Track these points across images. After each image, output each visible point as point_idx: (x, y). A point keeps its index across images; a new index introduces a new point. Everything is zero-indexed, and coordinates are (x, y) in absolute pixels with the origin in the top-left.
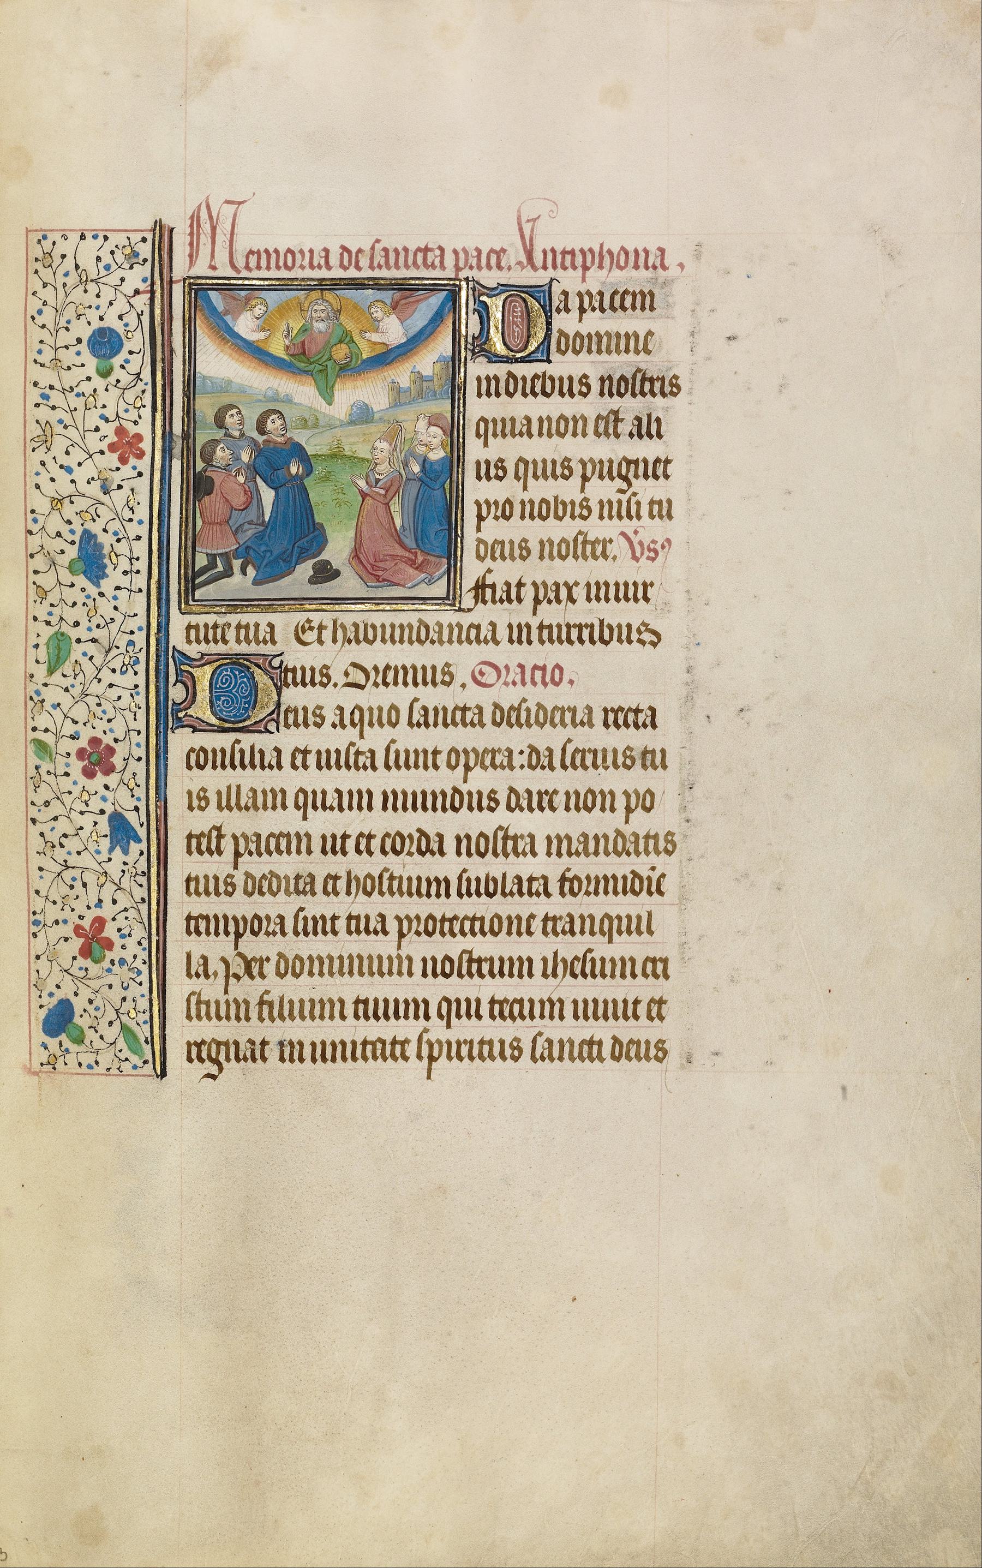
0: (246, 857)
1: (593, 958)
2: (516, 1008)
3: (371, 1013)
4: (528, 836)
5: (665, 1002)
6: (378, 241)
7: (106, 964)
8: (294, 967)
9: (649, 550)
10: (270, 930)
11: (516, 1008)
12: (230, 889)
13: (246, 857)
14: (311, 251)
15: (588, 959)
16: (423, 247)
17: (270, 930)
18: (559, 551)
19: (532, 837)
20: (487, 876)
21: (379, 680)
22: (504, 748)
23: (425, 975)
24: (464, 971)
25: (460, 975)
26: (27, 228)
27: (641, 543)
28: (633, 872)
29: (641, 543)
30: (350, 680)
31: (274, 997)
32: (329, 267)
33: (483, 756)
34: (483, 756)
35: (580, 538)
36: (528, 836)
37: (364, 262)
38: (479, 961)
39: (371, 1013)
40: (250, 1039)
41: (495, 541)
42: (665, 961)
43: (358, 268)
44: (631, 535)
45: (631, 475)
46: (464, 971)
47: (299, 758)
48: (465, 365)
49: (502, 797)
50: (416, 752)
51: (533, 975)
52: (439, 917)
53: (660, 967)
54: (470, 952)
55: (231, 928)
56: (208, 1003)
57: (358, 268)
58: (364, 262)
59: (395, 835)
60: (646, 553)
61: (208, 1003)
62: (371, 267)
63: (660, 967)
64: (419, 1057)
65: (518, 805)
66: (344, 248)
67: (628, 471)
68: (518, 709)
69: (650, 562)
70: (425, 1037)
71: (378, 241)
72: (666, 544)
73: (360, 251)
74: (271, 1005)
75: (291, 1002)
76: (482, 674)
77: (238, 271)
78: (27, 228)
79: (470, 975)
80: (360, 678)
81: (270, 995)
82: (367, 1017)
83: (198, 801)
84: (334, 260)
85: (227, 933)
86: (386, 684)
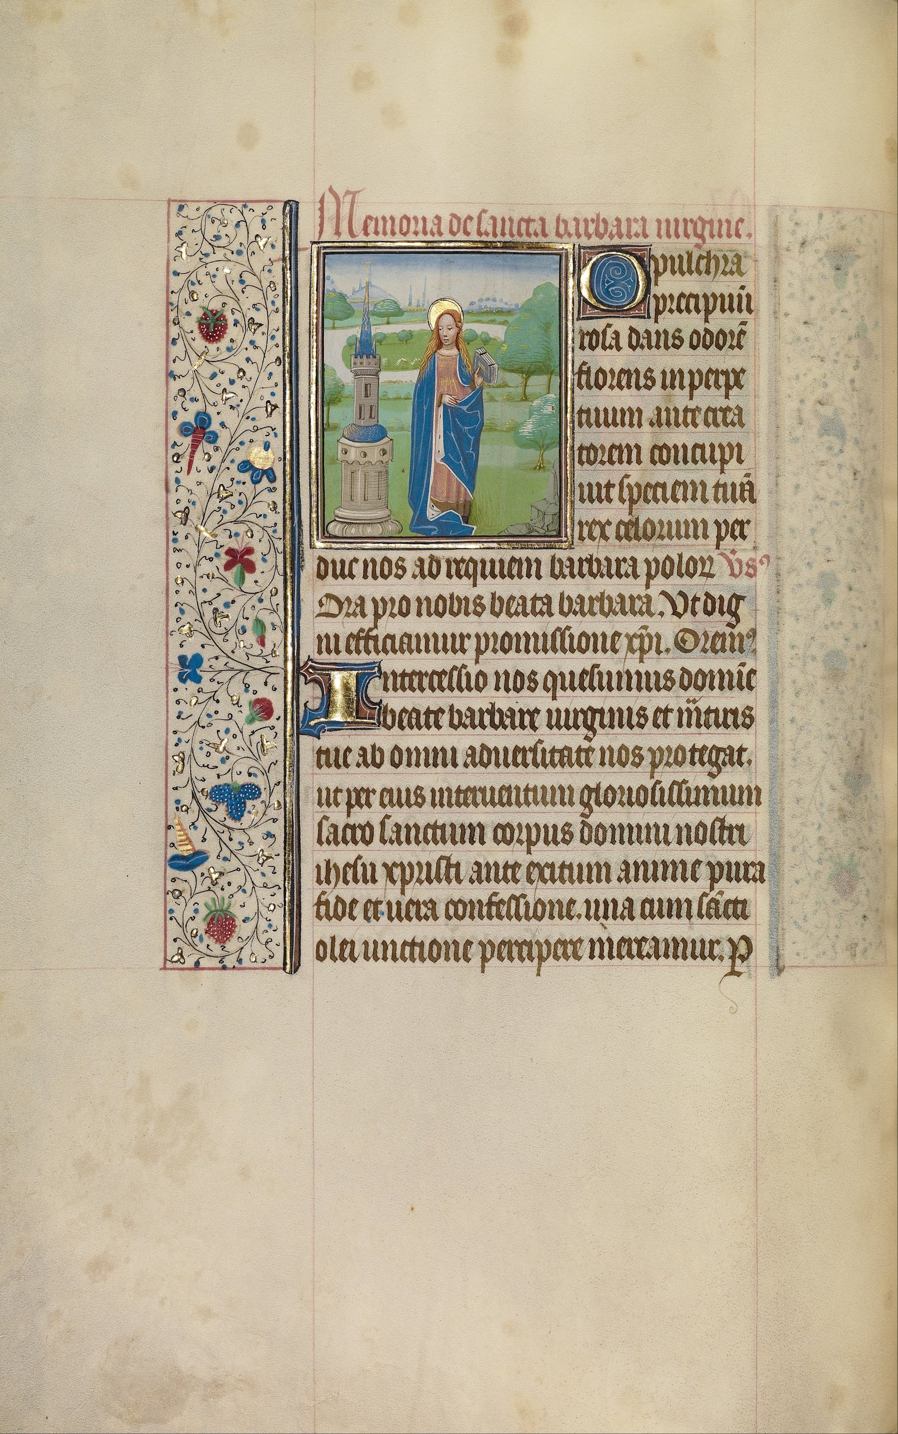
0: (666, 313)
1: (363, 863)
2: (692, 302)
4: (630, 559)
6: (484, 211)
7: (222, 551)
8: (597, 835)
10: (728, 269)
11: (692, 302)
13: (357, 808)
14: (424, 219)
16: (410, 941)
17: (728, 269)
19: (543, 220)
21: (708, 646)
24: (717, 837)
25: (713, 841)
26: (161, 969)
28: (683, 669)
30: (323, 610)
32: (495, 235)
36: (630, 559)
37: (472, 227)
38: (730, 828)
40: (628, 898)
43: (467, 233)
46: (717, 837)
48: (285, 710)
49: (487, 602)
51: (761, 803)
52: (423, 710)
54: (722, 821)
55: (717, 456)
57: (467, 233)
58: (472, 227)
59: (469, 561)
62: (479, 233)
64: (622, 500)
65: (611, 610)
66: (454, 216)
67: (589, 798)
68: (355, 866)
69: (640, 745)
70: (626, 481)
71: (484, 211)
73: (470, 218)
76: (684, 641)
78: (161, 969)
79: (722, 842)
80: (333, 607)
84: (445, 228)
85: (682, 387)
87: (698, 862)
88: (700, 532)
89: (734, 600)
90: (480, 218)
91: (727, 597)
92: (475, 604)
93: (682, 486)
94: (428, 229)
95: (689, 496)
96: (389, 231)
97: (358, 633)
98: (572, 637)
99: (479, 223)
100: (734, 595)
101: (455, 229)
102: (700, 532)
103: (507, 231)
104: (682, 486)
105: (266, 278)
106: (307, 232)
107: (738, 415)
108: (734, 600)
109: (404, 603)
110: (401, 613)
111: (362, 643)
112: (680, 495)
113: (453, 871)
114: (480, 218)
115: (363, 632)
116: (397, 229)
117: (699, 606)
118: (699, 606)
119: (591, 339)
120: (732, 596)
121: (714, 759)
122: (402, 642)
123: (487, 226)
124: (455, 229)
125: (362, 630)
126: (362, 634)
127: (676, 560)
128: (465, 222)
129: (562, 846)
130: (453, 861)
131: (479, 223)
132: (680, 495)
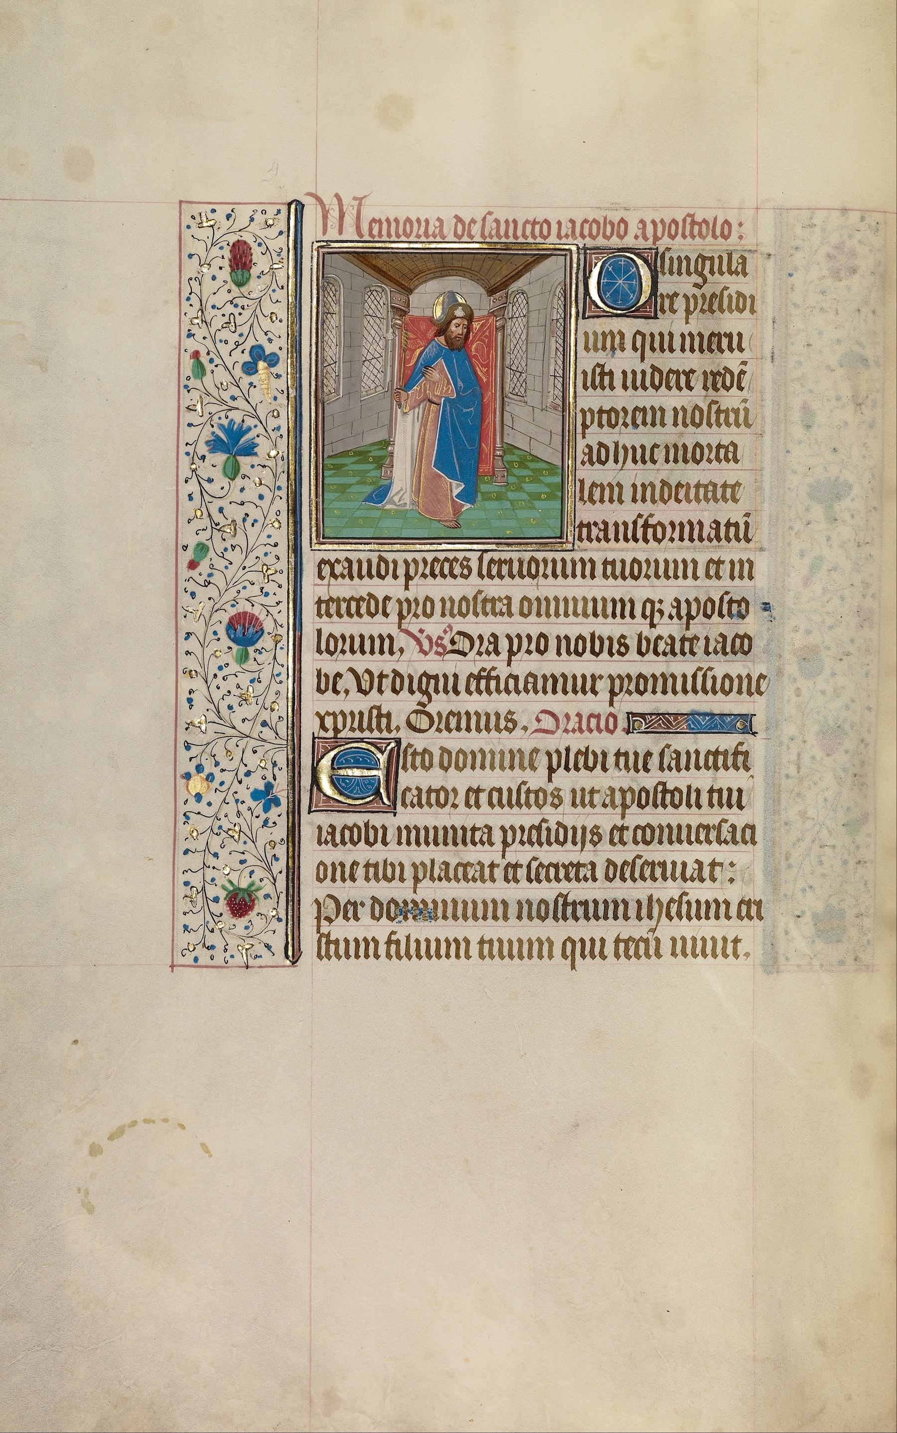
3: (403, 952)
5: (740, 940)
6: (490, 213)
9: (438, 645)
10: (570, 727)
12: (623, 650)
15: (684, 902)
17: (570, 727)
18: (404, 230)
20: (385, 861)
22: (413, 787)
23: (674, 954)
27: (429, 639)
29: (429, 639)
30: (456, 647)
31: (401, 936)
32: (498, 235)
33: (668, 376)
34: (668, 376)
35: (375, 712)
37: (476, 230)
39: (403, 952)
41: (349, 902)
42: (759, 904)
44: (418, 635)
45: (431, 690)
47: (617, 835)
50: (356, 941)
53: (754, 909)
56: (337, 942)
58: (476, 230)
60: (435, 648)
61: (337, 942)
62: (483, 235)
63: (754, 909)
66: (459, 219)
71: (490, 213)
72: (448, 629)
73: (473, 221)
74: (398, 942)
75: (418, 942)
77: (361, 235)
81: (745, 745)
82: (399, 957)
83: (324, 873)
86: (483, 881)
87: (536, 751)
88: (500, 912)
89: (424, 680)
90: (484, 219)
91: (693, 257)
92: (620, 644)
93: (599, 488)
94: (430, 232)
95: (606, 498)
96: (393, 232)
97: (480, 672)
98: (714, 678)
99: (483, 226)
100: (700, 256)
101: (460, 231)
102: (500, 912)
103: (393, 232)
104: (599, 488)
105: (272, 423)
106: (311, 232)
107: (604, 530)
108: (424, 680)
109: (429, 604)
110: (425, 614)
111: (483, 683)
112: (597, 496)
113: (384, 721)
114: (484, 219)
115: (485, 671)
116: (401, 231)
117: (387, 683)
118: (387, 683)
119: (541, 227)
120: (698, 257)
121: (424, 687)
122: (526, 682)
123: (490, 224)
124: (460, 231)
125: (484, 669)
126: (483, 674)
127: (685, 791)
128: (470, 225)
129: (460, 580)
130: (332, 938)
131: (483, 226)
132: (597, 496)
